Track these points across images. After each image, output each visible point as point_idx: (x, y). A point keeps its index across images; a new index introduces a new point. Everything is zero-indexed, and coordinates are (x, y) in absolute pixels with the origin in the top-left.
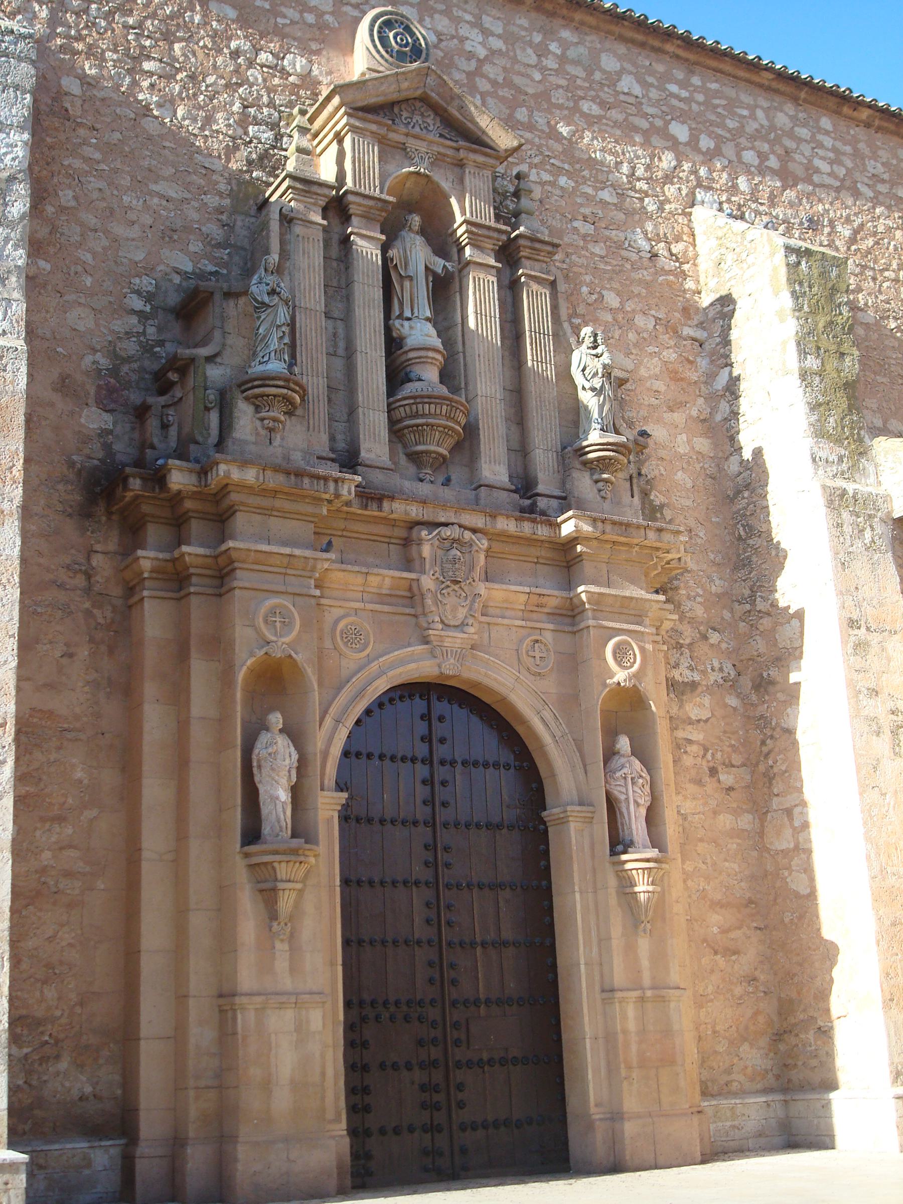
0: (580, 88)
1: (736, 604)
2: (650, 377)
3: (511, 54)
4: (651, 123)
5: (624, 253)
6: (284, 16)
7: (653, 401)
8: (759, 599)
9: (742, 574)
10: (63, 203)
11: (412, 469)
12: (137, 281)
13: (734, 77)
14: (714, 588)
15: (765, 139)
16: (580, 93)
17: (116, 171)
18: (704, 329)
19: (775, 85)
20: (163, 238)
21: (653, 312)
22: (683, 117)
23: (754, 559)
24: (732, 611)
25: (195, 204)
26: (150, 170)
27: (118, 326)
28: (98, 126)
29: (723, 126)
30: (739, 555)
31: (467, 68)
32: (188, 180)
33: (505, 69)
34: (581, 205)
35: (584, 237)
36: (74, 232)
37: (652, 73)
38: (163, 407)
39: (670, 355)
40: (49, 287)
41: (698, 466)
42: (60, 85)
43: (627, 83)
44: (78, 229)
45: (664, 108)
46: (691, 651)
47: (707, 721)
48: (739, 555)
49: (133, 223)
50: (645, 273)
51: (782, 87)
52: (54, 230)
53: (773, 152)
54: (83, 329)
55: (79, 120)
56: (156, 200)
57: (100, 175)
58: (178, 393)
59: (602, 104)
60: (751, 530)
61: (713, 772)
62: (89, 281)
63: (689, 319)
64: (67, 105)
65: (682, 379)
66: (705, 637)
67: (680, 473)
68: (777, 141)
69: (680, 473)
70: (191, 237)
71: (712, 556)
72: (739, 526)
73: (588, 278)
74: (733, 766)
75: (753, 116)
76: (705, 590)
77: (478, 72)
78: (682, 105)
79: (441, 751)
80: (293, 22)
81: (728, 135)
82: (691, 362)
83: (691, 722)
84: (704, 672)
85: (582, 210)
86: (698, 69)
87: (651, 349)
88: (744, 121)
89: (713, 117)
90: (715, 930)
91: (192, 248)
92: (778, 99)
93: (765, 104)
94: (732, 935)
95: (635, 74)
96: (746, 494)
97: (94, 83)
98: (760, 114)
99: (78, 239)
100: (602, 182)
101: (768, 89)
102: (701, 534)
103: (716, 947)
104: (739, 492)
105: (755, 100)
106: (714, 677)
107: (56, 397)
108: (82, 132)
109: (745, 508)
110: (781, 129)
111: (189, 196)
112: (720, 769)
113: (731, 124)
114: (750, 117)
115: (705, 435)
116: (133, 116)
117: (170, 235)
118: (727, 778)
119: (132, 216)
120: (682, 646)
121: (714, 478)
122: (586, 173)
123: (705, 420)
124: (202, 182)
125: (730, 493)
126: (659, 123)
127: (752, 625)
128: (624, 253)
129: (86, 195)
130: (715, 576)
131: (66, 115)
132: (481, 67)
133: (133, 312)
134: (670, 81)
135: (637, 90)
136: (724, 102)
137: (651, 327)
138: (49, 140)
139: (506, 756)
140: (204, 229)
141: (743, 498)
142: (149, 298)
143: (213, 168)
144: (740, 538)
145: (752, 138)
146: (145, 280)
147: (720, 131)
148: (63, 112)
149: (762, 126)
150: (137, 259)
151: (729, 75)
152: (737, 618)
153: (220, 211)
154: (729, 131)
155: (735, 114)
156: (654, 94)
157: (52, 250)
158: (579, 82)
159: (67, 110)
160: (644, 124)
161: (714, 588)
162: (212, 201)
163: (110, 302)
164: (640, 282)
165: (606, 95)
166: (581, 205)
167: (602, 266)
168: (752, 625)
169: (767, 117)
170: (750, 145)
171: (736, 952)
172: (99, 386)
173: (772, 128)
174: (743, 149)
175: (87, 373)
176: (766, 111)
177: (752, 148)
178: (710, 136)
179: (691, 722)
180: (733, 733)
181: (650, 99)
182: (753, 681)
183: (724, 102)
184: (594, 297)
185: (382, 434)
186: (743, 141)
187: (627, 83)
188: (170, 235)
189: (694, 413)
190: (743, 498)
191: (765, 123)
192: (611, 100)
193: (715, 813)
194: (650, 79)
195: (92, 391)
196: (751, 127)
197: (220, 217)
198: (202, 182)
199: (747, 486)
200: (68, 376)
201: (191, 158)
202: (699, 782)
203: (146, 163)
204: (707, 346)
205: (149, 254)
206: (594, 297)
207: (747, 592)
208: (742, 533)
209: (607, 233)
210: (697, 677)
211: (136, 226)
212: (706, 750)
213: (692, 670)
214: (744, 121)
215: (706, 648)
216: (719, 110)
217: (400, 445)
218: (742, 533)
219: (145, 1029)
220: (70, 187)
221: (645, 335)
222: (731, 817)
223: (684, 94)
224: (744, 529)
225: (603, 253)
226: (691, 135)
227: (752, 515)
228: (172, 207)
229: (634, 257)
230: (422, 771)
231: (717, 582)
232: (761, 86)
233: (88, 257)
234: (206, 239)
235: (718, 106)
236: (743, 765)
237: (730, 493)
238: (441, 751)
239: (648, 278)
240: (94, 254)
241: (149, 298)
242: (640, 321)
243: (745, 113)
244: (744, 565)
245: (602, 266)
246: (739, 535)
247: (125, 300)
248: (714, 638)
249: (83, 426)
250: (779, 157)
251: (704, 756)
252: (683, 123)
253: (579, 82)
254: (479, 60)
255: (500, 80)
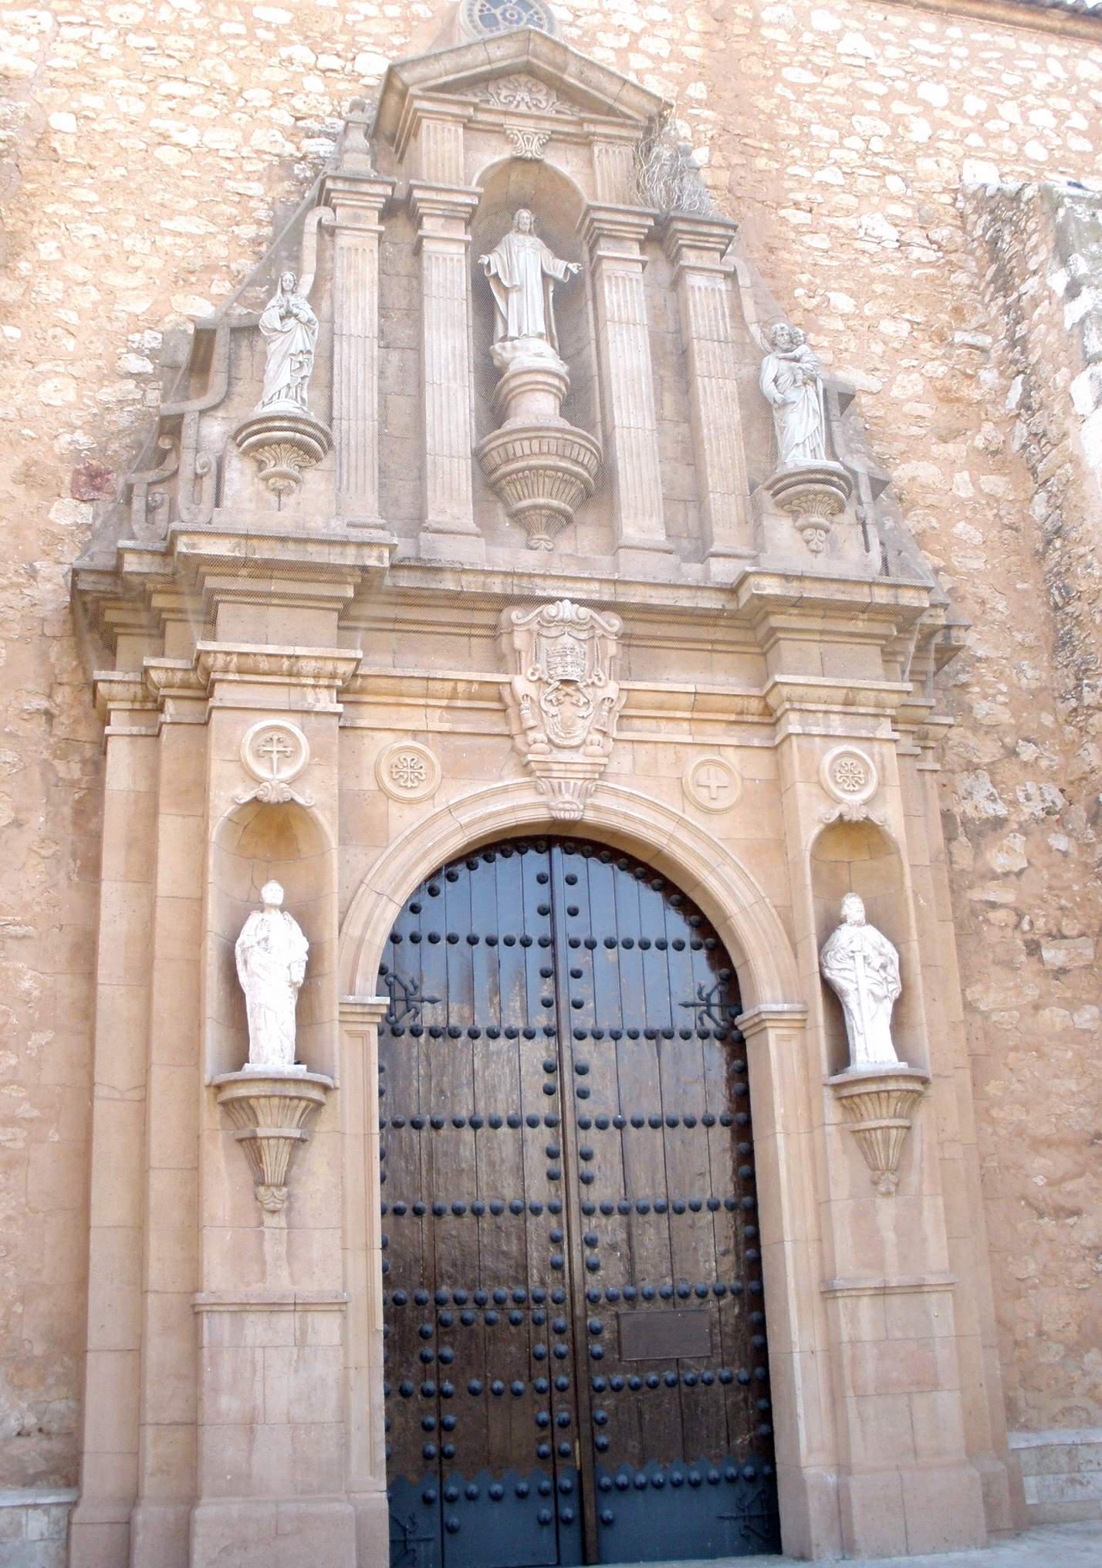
0: (784, 53)
1: (1059, 701)
2: (908, 400)
3: (680, 23)
4: (891, 88)
5: (859, 245)
6: (357, 12)
7: (915, 430)
8: (1086, 689)
9: (1062, 658)
10: (44, 257)
11: (519, 536)
12: (137, 337)
13: (1009, 22)
14: (1024, 681)
15: (1063, 94)
16: (785, 59)
17: (117, 212)
18: (987, 333)
19: (1071, 25)
20: (176, 283)
21: (907, 316)
22: (937, 76)
23: (1076, 632)
24: (1054, 712)
25: (224, 238)
26: (163, 205)
27: (108, 394)
28: (95, 163)
29: (998, 82)
30: (1057, 631)
31: (616, 44)
32: (215, 211)
33: (671, 41)
34: (791, 190)
35: (796, 229)
36: (52, 290)
37: (889, 29)
38: (149, 484)
39: (938, 369)
40: (17, 358)
41: (990, 514)
42: (47, 123)
43: (853, 43)
44: (60, 285)
45: (909, 68)
46: (992, 773)
47: (1021, 872)
48: (1057, 631)
49: (137, 269)
50: (891, 267)
51: (1082, 27)
52: (28, 290)
53: (1076, 108)
54: (60, 403)
55: (71, 160)
56: (169, 240)
57: (95, 219)
58: (170, 464)
59: (817, 70)
60: (1068, 593)
61: (1033, 948)
62: (70, 344)
63: (963, 320)
64: (56, 145)
65: (958, 400)
66: (1013, 753)
67: (961, 525)
68: (1082, 94)
69: (961, 525)
70: (216, 277)
71: (1019, 637)
72: (1054, 590)
73: (805, 278)
74: (1064, 937)
75: (1043, 68)
76: (1011, 686)
77: (633, 46)
78: (935, 62)
79: (568, 928)
80: (367, 18)
81: (1005, 93)
82: (970, 377)
83: (995, 877)
84: (1013, 803)
85: (792, 196)
86: (955, 18)
87: (905, 363)
88: (1030, 75)
89: (983, 74)
90: (1040, 1181)
91: (215, 290)
92: (1078, 46)
93: (1062, 52)
94: (1069, 1186)
95: (864, 33)
96: (1058, 543)
97: (92, 115)
98: (1053, 65)
99: (60, 296)
100: (821, 160)
101: (1063, 33)
102: (1000, 607)
103: (1042, 1205)
104: (1049, 542)
105: (1045, 49)
106: (1036, 808)
107: (19, 491)
108: (74, 173)
109: (1058, 564)
110: (1086, 80)
111: (213, 229)
112: (1043, 941)
113: (1009, 79)
114: (1039, 69)
115: (998, 471)
116: (143, 146)
117: (184, 278)
118: (1052, 955)
119: (135, 261)
120: (977, 767)
121: (1017, 530)
122: (797, 152)
123: (995, 453)
124: (235, 211)
125: (1040, 546)
126: (901, 85)
127: (1081, 729)
128: (859, 245)
129: (75, 245)
130: (1025, 665)
131: (54, 156)
132: (636, 41)
133: (130, 375)
134: (915, 36)
135: (868, 49)
136: (998, 55)
137: (904, 334)
138: (29, 187)
139: (678, 927)
140: (233, 266)
141: (1056, 550)
142: (153, 354)
143: (250, 193)
144: (1056, 608)
145: (1045, 94)
146: (148, 334)
147: (992, 89)
148: (51, 154)
149: (1058, 79)
150: (138, 311)
151: (1003, 21)
152: (1061, 720)
153: (256, 241)
154: (1009, 88)
155: (1016, 67)
156: (892, 52)
157: (23, 313)
158: (780, 47)
159: (55, 150)
160: (880, 89)
161: (1024, 681)
162: (248, 231)
163: (99, 367)
164: (884, 279)
165: (821, 59)
166: (791, 190)
167: (825, 262)
168: (1081, 729)
169: (1065, 69)
170: (1041, 103)
171: (1076, 1213)
172: (77, 472)
173: (1073, 79)
174: (1031, 109)
175: (61, 458)
176: (1063, 60)
177: (1046, 106)
178: (979, 96)
179: (995, 877)
180: (1064, 889)
181: (887, 60)
182: (1088, 810)
183: (998, 55)
184: (815, 302)
185: (464, 487)
186: (1030, 99)
187: (853, 43)
188: (184, 278)
189: (979, 443)
190: (1056, 550)
191: (1063, 76)
192: (830, 64)
193: (1037, 1007)
194: (885, 36)
195: (68, 479)
196: (1040, 81)
197: (257, 249)
198: (235, 211)
199: (1058, 532)
200: (36, 463)
201: (220, 186)
202: (1010, 965)
203: (157, 199)
204: (994, 355)
205: (156, 302)
206: (815, 302)
207: (1071, 682)
208: (1058, 599)
209: (830, 221)
210: (1001, 810)
211: (140, 273)
212: (1020, 916)
213: (994, 801)
214: (1030, 75)
215: (1016, 769)
216: (990, 64)
217: (500, 505)
218: (1058, 599)
219: (94, 1339)
220: (54, 237)
221: (896, 345)
222: (1063, 1012)
223: (936, 49)
224: (1060, 593)
225: (826, 245)
226: (951, 97)
227: (1068, 570)
228: (190, 245)
229: (872, 247)
230: (537, 957)
231: (1030, 673)
232: (1051, 31)
233: (73, 318)
234: (236, 277)
235: (989, 60)
236: (1082, 935)
237: (1040, 546)
238: (568, 928)
239: (897, 273)
240: (80, 313)
241: (153, 354)
242: (887, 327)
243: (1033, 65)
244: (1065, 644)
245: (825, 262)
246: (1056, 603)
247: (120, 362)
248: (1028, 752)
249: (52, 523)
250: (1085, 114)
251: (1017, 926)
252: (939, 83)
253: (780, 47)
254: (633, 33)
255: (665, 53)
